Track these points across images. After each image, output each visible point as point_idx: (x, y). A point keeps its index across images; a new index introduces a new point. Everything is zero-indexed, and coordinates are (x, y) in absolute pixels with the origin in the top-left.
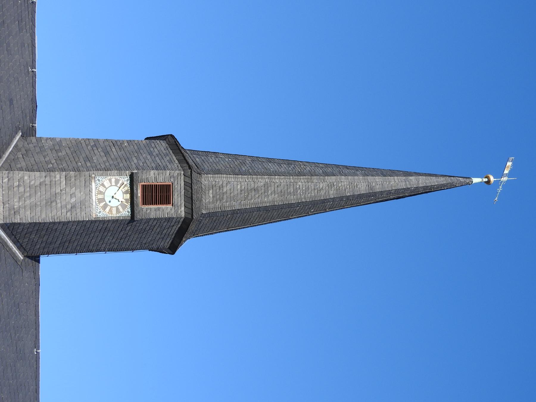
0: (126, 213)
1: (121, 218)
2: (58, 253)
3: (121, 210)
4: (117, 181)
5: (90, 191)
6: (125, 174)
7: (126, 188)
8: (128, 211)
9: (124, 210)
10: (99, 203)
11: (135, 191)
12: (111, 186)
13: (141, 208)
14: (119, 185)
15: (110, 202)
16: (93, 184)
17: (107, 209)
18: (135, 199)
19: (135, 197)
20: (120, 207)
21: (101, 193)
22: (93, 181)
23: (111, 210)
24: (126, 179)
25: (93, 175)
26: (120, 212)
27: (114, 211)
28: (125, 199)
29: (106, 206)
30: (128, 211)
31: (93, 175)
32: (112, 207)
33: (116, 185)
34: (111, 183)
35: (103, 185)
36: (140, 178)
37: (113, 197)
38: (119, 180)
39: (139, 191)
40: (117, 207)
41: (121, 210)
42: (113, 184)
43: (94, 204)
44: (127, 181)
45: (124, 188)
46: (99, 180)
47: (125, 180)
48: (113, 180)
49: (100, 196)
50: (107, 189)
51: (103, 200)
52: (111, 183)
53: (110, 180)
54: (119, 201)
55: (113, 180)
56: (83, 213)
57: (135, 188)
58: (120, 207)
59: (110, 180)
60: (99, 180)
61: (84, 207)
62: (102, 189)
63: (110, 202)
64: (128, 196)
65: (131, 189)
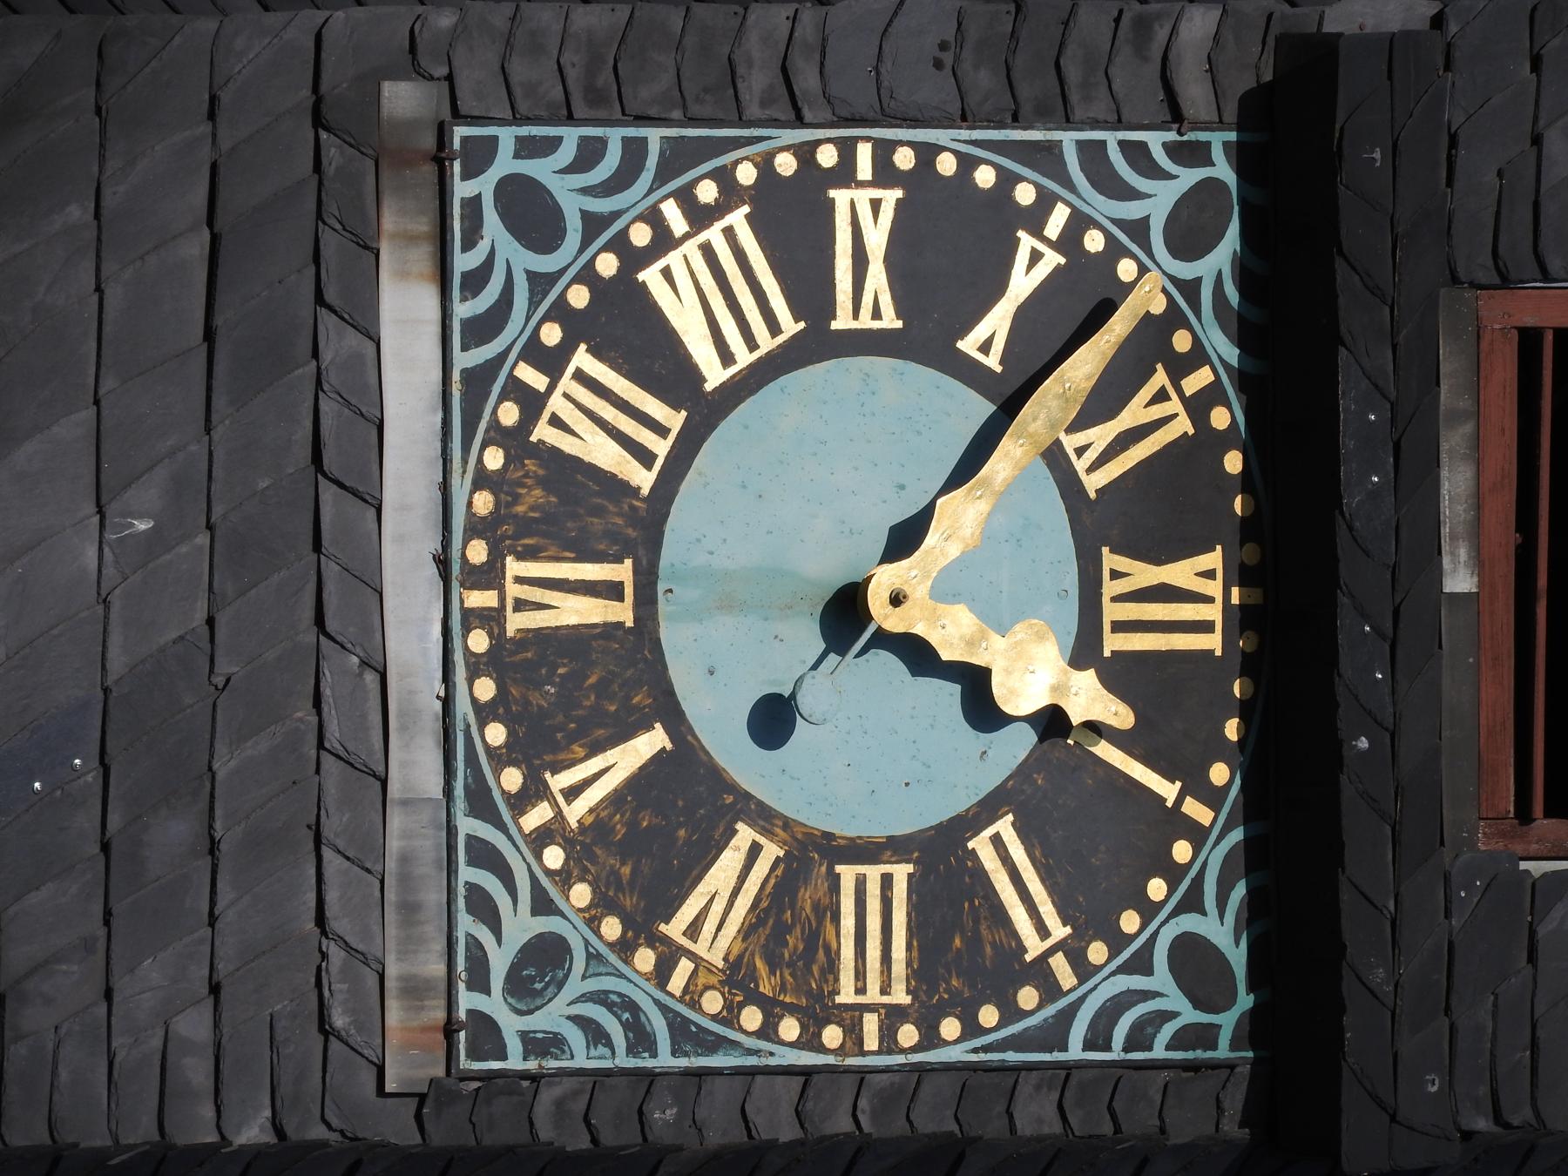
0: (1132, 981)
1: (1036, 1115)
2: (713, 427)
3: (1034, 920)
4: (948, 253)
5: (341, 464)
6: (1135, 79)
7: (1160, 415)
8: (1193, 959)
9: (1090, 916)
10: (540, 747)
11: (1365, 482)
12: (818, 343)
13: (1506, 887)
14: (989, 334)
15: (773, 720)
16: (407, 311)
17: (724, 894)
18: (1362, 667)
19: (1356, 633)
20: (1001, 852)
21: (568, 508)
22: (399, 223)
23: (790, 930)
24: (1158, 201)
25: (403, 99)
26: (1006, 970)
27: (872, 951)
28: (1122, 675)
29: (680, 814)
30: (1193, 959)
31: (403, 99)
32: (812, 854)
33: (927, 336)
34: (809, 285)
35: (630, 331)
36: (1480, 169)
37: (845, 615)
38: (998, 223)
39: (1455, 484)
40: (941, 858)
41: (1034, 920)
42: (867, 299)
43: (416, 767)
44: (1189, 235)
45: (1101, 402)
46: (531, 214)
47: (1132, 216)
48: (865, 216)
49: (564, 597)
50: (706, 411)
51: (613, 678)
52: (809, 285)
53: (795, 227)
54: (981, 708)
55: (865, 216)
56: (149, 981)
57: (1360, 414)
58: (1001, 852)
59: (795, 227)
60: (531, 214)
61: (174, 832)
62: (594, 421)
63: (773, 720)
64: (1193, 599)
65: (1260, 437)
